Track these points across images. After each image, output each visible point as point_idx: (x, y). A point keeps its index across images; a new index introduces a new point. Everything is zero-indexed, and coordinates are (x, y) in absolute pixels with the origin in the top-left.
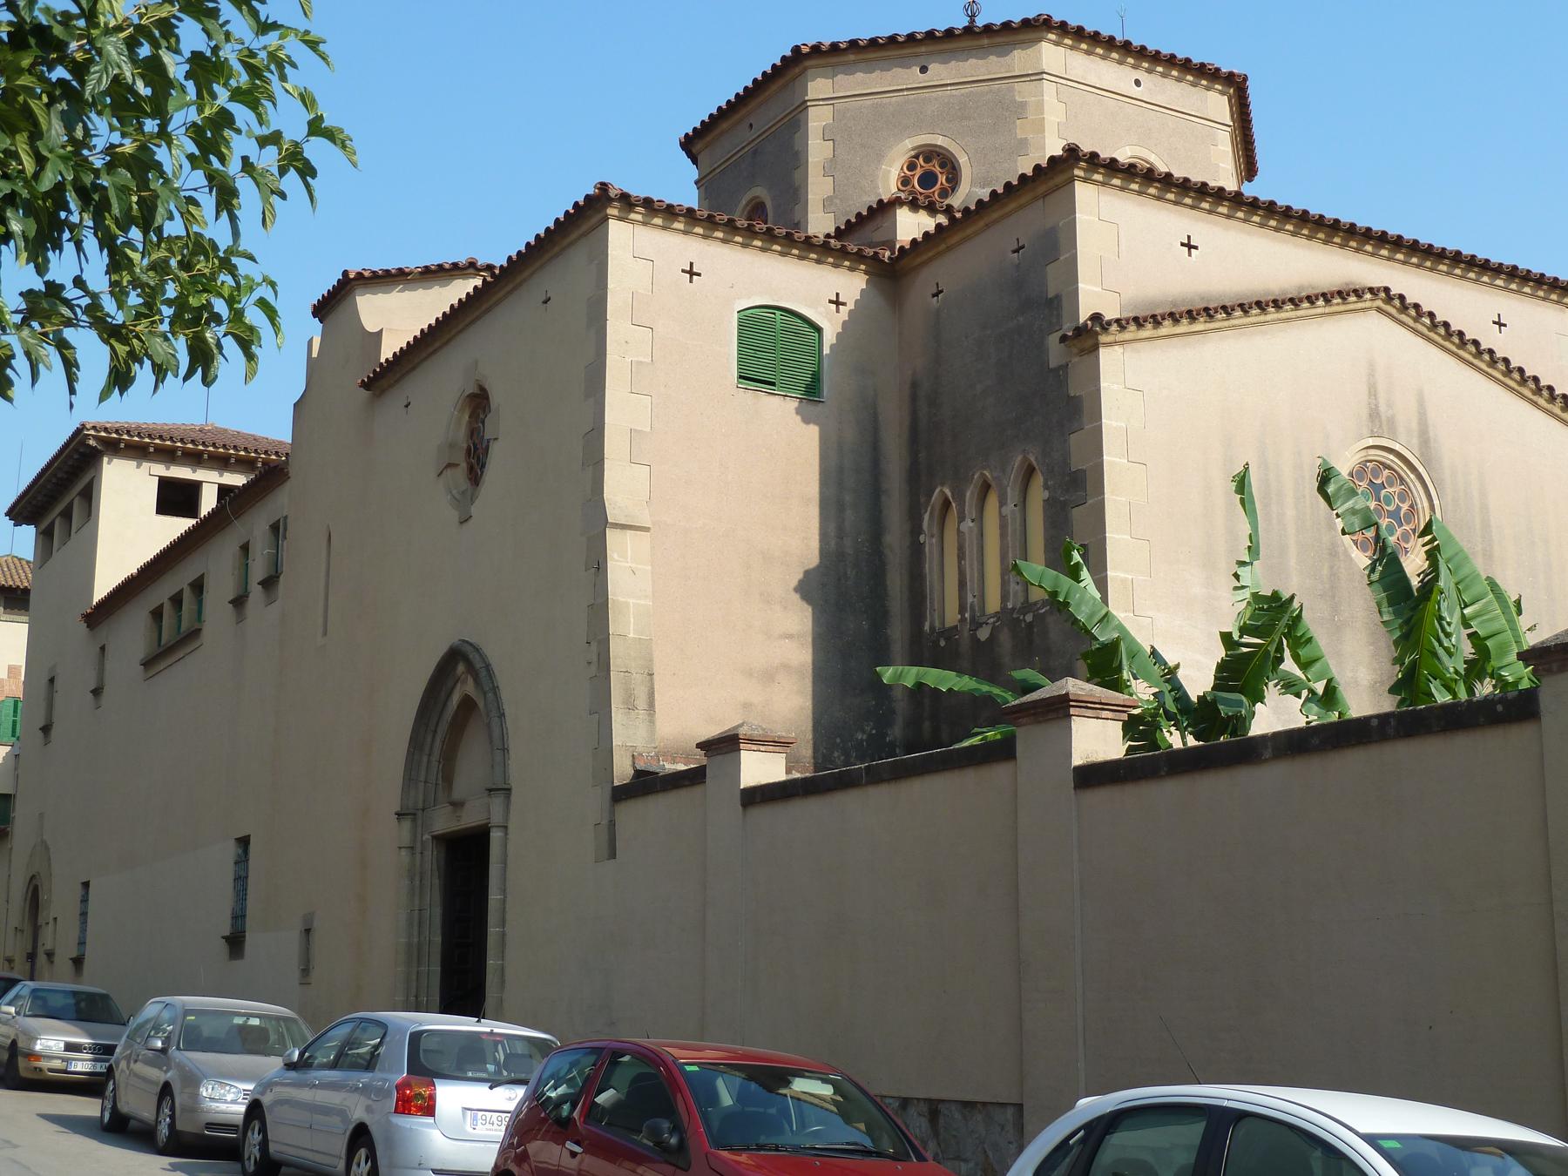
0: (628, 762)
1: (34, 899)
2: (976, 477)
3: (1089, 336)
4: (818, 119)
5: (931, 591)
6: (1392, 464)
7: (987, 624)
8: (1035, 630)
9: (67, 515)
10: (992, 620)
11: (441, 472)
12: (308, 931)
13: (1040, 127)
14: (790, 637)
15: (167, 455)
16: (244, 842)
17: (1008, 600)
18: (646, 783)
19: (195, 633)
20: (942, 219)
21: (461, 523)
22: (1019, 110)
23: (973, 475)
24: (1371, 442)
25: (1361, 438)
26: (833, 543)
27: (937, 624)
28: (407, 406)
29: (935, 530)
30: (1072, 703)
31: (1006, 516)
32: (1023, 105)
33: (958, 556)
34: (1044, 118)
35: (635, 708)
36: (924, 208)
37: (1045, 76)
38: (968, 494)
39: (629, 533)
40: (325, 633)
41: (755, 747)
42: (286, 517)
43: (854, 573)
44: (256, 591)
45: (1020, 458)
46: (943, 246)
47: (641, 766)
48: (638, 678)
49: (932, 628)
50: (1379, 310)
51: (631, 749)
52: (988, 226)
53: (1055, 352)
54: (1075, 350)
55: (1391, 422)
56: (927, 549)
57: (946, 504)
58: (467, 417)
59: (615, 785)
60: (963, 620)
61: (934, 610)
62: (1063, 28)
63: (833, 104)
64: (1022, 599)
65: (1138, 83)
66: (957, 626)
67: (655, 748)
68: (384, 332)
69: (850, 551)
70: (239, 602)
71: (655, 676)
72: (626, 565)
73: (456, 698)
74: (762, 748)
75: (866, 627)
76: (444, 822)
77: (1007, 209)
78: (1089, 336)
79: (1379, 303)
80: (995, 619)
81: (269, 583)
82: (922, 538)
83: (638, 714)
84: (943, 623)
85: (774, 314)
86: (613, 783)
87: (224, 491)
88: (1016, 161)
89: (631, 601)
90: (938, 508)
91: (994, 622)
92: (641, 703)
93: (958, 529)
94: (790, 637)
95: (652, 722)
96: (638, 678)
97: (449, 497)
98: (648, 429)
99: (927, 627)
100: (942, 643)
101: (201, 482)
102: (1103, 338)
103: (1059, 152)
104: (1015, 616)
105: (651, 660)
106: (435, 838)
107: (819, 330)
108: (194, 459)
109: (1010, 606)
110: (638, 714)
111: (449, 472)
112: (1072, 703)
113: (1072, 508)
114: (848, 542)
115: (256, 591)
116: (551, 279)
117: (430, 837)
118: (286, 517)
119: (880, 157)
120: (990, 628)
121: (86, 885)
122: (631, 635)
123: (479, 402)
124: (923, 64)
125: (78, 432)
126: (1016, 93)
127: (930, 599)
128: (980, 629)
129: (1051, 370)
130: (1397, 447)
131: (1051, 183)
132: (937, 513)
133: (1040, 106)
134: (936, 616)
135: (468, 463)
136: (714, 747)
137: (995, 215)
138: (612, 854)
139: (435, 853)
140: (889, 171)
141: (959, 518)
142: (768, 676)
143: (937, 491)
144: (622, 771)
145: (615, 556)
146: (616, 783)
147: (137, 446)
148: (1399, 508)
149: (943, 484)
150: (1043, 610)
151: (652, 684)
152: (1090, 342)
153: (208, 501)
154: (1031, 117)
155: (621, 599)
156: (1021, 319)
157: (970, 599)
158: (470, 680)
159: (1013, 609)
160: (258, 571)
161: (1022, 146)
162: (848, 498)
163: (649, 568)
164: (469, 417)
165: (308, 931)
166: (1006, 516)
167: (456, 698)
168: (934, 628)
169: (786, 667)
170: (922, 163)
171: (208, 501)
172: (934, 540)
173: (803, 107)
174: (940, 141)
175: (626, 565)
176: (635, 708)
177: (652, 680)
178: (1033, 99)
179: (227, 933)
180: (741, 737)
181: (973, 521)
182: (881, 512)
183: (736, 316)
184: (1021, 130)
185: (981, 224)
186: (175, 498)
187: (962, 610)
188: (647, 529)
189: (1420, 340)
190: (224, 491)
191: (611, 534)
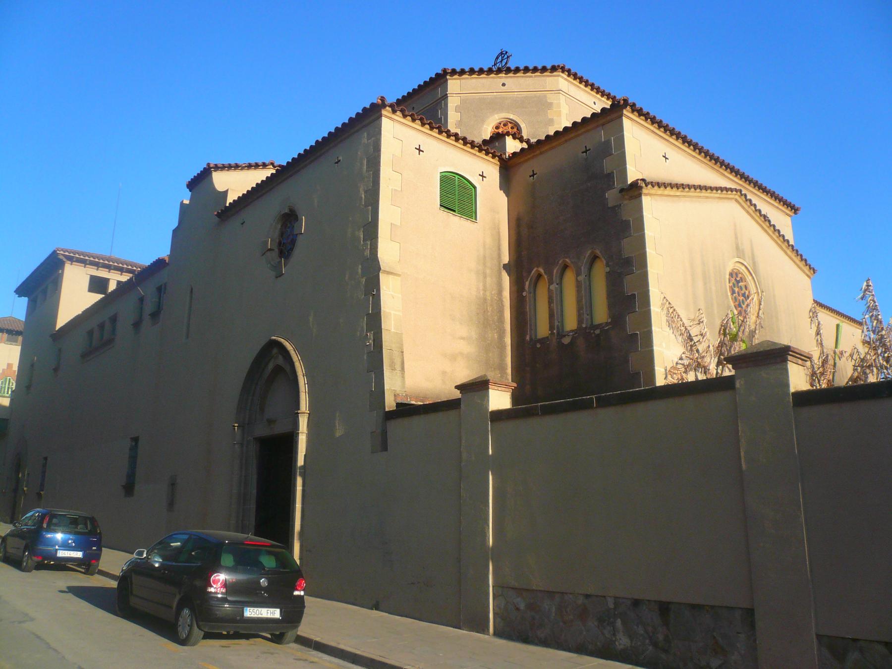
0: (392, 398)
1: (18, 466)
2: (560, 262)
3: (635, 190)
4: (453, 103)
5: (530, 320)
6: (743, 272)
7: (569, 335)
8: (602, 338)
9: (45, 292)
10: (571, 334)
11: (264, 254)
12: (173, 484)
13: (559, 114)
14: (463, 338)
15: (97, 265)
16: (136, 440)
17: (583, 323)
18: (405, 410)
19: (110, 341)
20: (525, 146)
21: (277, 277)
22: (550, 105)
23: (559, 261)
24: (737, 260)
25: (734, 257)
26: (481, 293)
27: (533, 337)
28: (242, 224)
29: (532, 290)
30: (791, 353)
31: (581, 281)
32: (551, 104)
33: (549, 302)
34: (560, 111)
35: (395, 369)
36: (518, 139)
37: (561, 92)
38: (555, 271)
39: (391, 277)
40: (187, 337)
41: (496, 388)
42: (165, 284)
43: (491, 309)
44: (147, 318)
45: (589, 252)
46: (538, 152)
47: (399, 401)
48: (396, 353)
49: (531, 339)
50: (736, 200)
51: (394, 392)
52: (566, 141)
53: (611, 196)
54: (626, 197)
55: (743, 252)
56: (527, 299)
57: (539, 276)
58: (280, 226)
59: (386, 410)
60: (552, 333)
61: (532, 329)
62: (569, 71)
63: (460, 97)
64: (590, 323)
65: (595, 103)
66: (548, 337)
67: (405, 391)
68: (229, 192)
69: (489, 298)
70: (137, 325)
71: (404, 353)
72: (390, 293)
73: (271, 366)
74: (500, 389)
75: (496, 337)
76: (262, 431)
77: (580, 132)
78: (635, 190)
79: (737, 197)
80: (574, 333)
81: (155, 315)
82: (524, 294)
83: (397, 373)
84: (536, 336)
85: (455, 177)
86: (385, 409)
87: (119, 283)
88: (548, 128)
89: (392, 312)
90: (534, 279)
91: (573, 335)
92: (398, 367)
93: (549, 288)
94: (463, 338)
95: (403, 377)
96: (396, 353)
97: (269, 265)
98: (399, 224)
99: (528, 338)
100: (538, 346)
101: (109, 279)
102: (644, 191)
103: (569, 125)
104: (587, 331)
105: (402, 345)
106: (255, 439)
107: (475, 188)
108: (109, 268)
109: (584, 326)
110: (397, 373)
111: (268, 253)
112: (791, 353)
113: (626, 275)
114: (488, 294)
115: (147, 318)
116: (340, 152)
117: (252, 439)
118: (165, 284)
119: (483, 121)
120: (570, 337)
121: (46, 459)
122: (393, 330)
123: (290, 218)
124: (505, 82)
125: (54, 252)
126: (548, 99)
127: (530, 324)
128: (564, 338)
129: (609, 208)
130: (745, 264)
131: (609, 118)
132: (533, 281)
133: (559, 105)
134: (533, 332)
135: (279, 249)
136: (468, 388)
137: (572, 135)
138: (384, 447)
139: (255, 446)
140: (488, 128)
141: (549, 282)
142: (453, 358)
143: (535, 270)
144: (390, 404)
145: (384, 287)
146: (387, 409)
147: (83, 260)
148: (745, 293)
149: (538, 267)
150: (607, 328)
151: (403, 358)
152: (636, 193)
153: (112, 287)
154: (554, 110)
155: (388, 311)
156: (589, 184)
157: (556, 323)
158: (280, 357)
159: (586, 328)
160: (149, 308)
161: (551, 122)
162: (488, 271)
163: (400, 296)
164: (281, 226)
165: (173, 484)
166: (581, 281)
167: (271, 366)
168: (532, 339)
169: (461, 354)
170: (503, 127)
171: (112, 287)
172: (532, 295)
173: (445, 97)
174: (512, 117)
175: (390, 293)
176: (395, 369)
177: (403, 355)
178: (555, 101)
179: (124, 484)
180: (491, 381)
181: (557, 284)
182: (502, 280)
183: (439, 175)
184: (550, 114)
185: (563, 139)
186: (97, 285)
187: (551, 328)
188: (399, 275)
189: (749, 217)
190: (119, 283)
191: (382, 277)
